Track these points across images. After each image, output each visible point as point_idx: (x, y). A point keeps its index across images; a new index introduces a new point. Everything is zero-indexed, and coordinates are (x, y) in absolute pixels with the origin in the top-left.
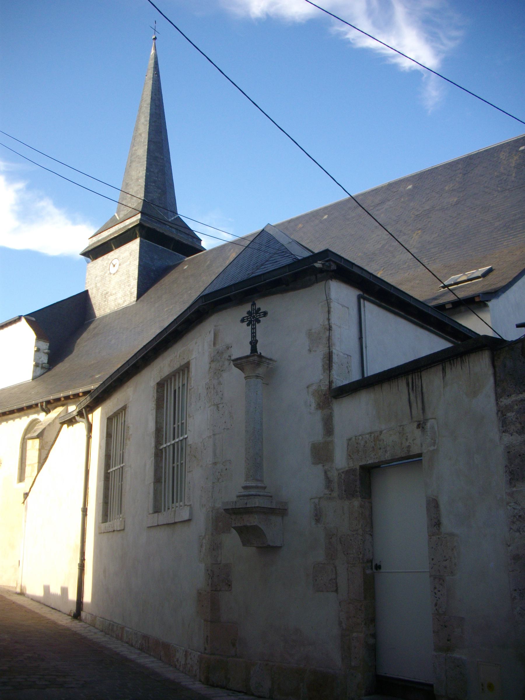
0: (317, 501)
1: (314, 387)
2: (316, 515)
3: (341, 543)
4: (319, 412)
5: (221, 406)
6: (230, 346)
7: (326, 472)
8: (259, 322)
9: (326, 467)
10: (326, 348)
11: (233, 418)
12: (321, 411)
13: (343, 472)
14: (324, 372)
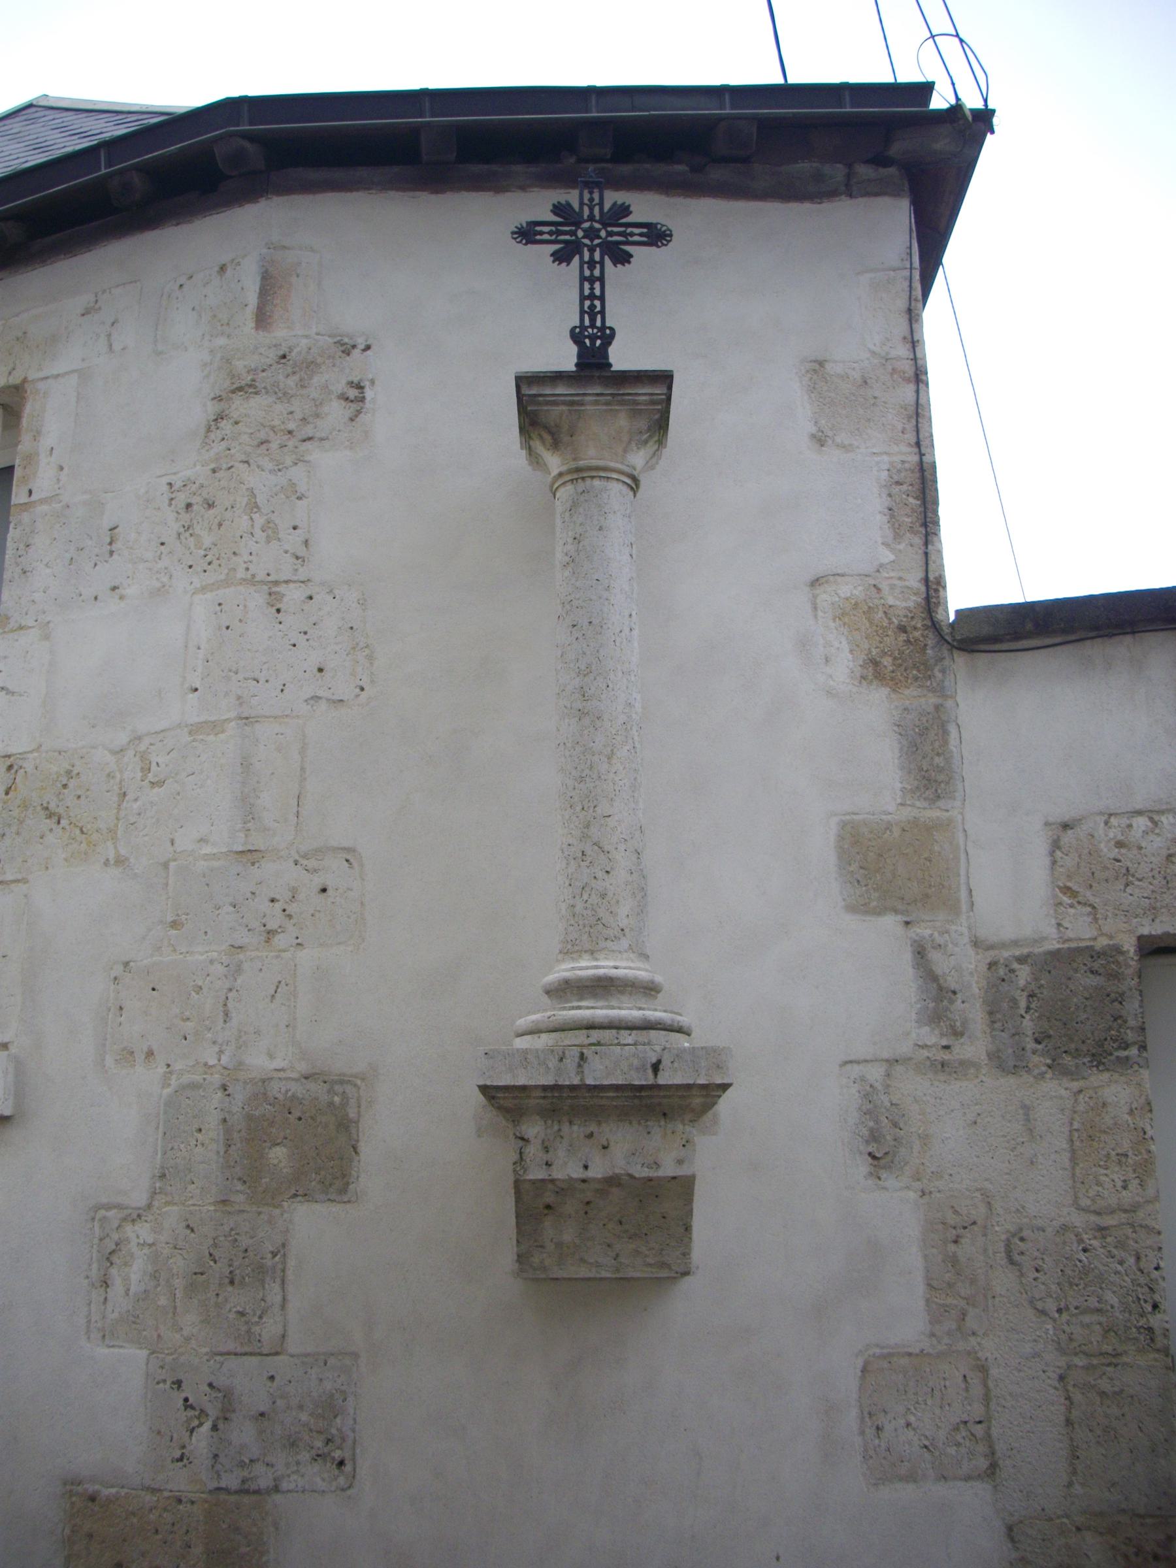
0: (875, 1073)
1: (847, 589)
2: (874, 1136)
3: (1012, 1262)
4: (879, 695)
5: (293, 595)
6: (361, 342)
7: (920, 952)
8: (623, 258)
9: (923, 931)
10: (904, 448)
11: (370, 658)
12: (885, 691)
13: (1022, 960)
14: (897, 536)
